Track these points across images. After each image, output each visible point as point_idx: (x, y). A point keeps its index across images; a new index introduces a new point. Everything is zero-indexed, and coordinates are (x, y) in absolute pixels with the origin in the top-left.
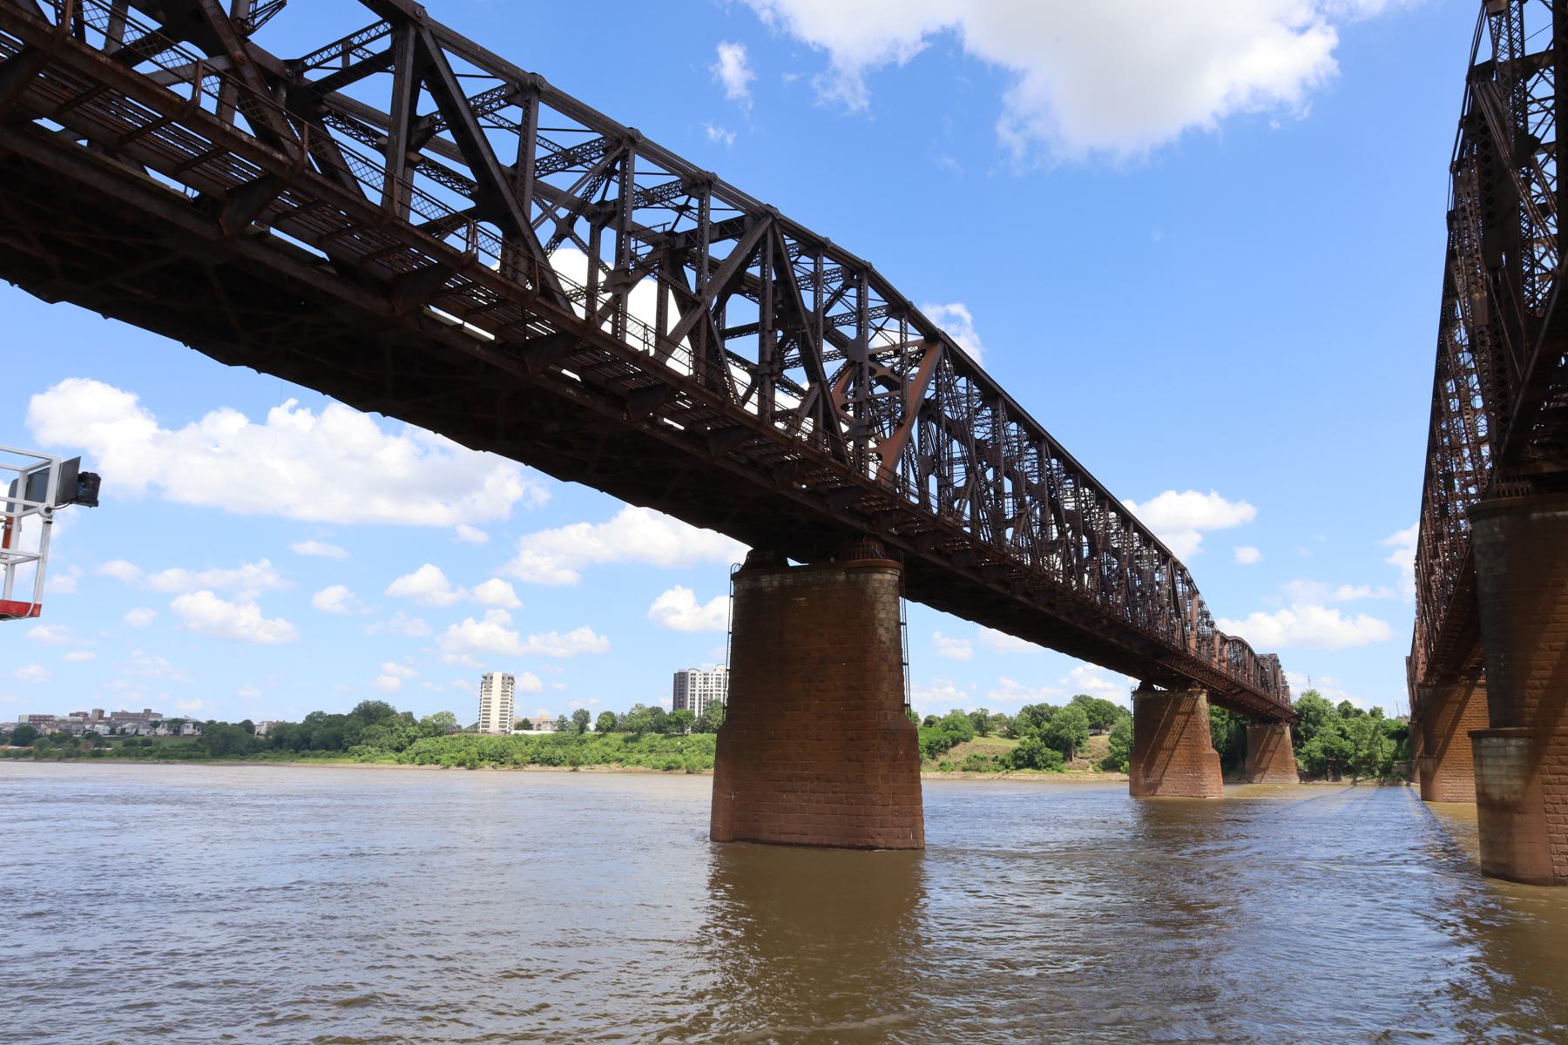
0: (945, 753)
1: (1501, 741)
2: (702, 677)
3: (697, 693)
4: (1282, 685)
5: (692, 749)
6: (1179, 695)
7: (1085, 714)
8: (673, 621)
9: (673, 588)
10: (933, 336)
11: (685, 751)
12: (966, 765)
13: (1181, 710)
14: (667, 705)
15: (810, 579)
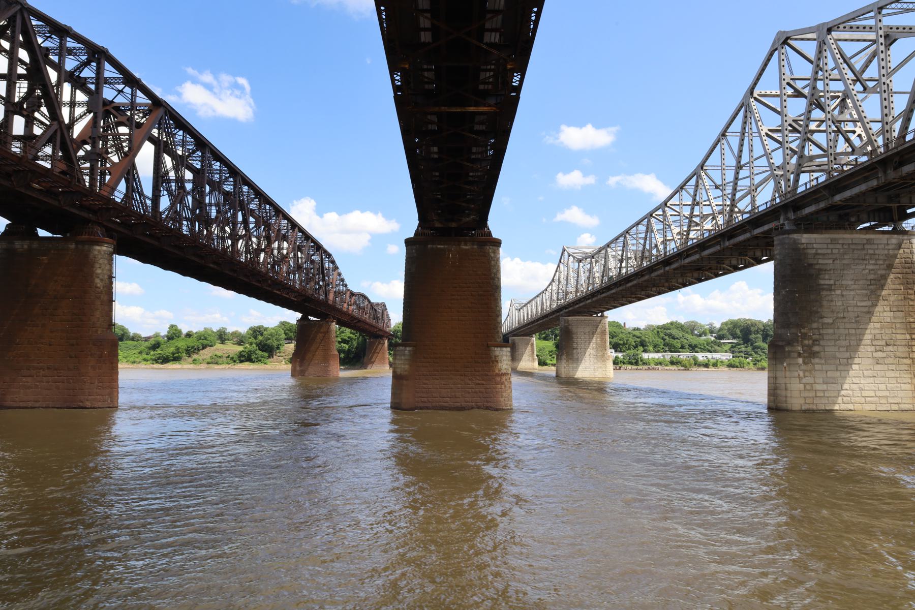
0: (197, 353)
1: (403, 348)
4: (386, 318)
7: (283, 332)
12: (210, 360)
13: (322, 331)
15: (50, 246)
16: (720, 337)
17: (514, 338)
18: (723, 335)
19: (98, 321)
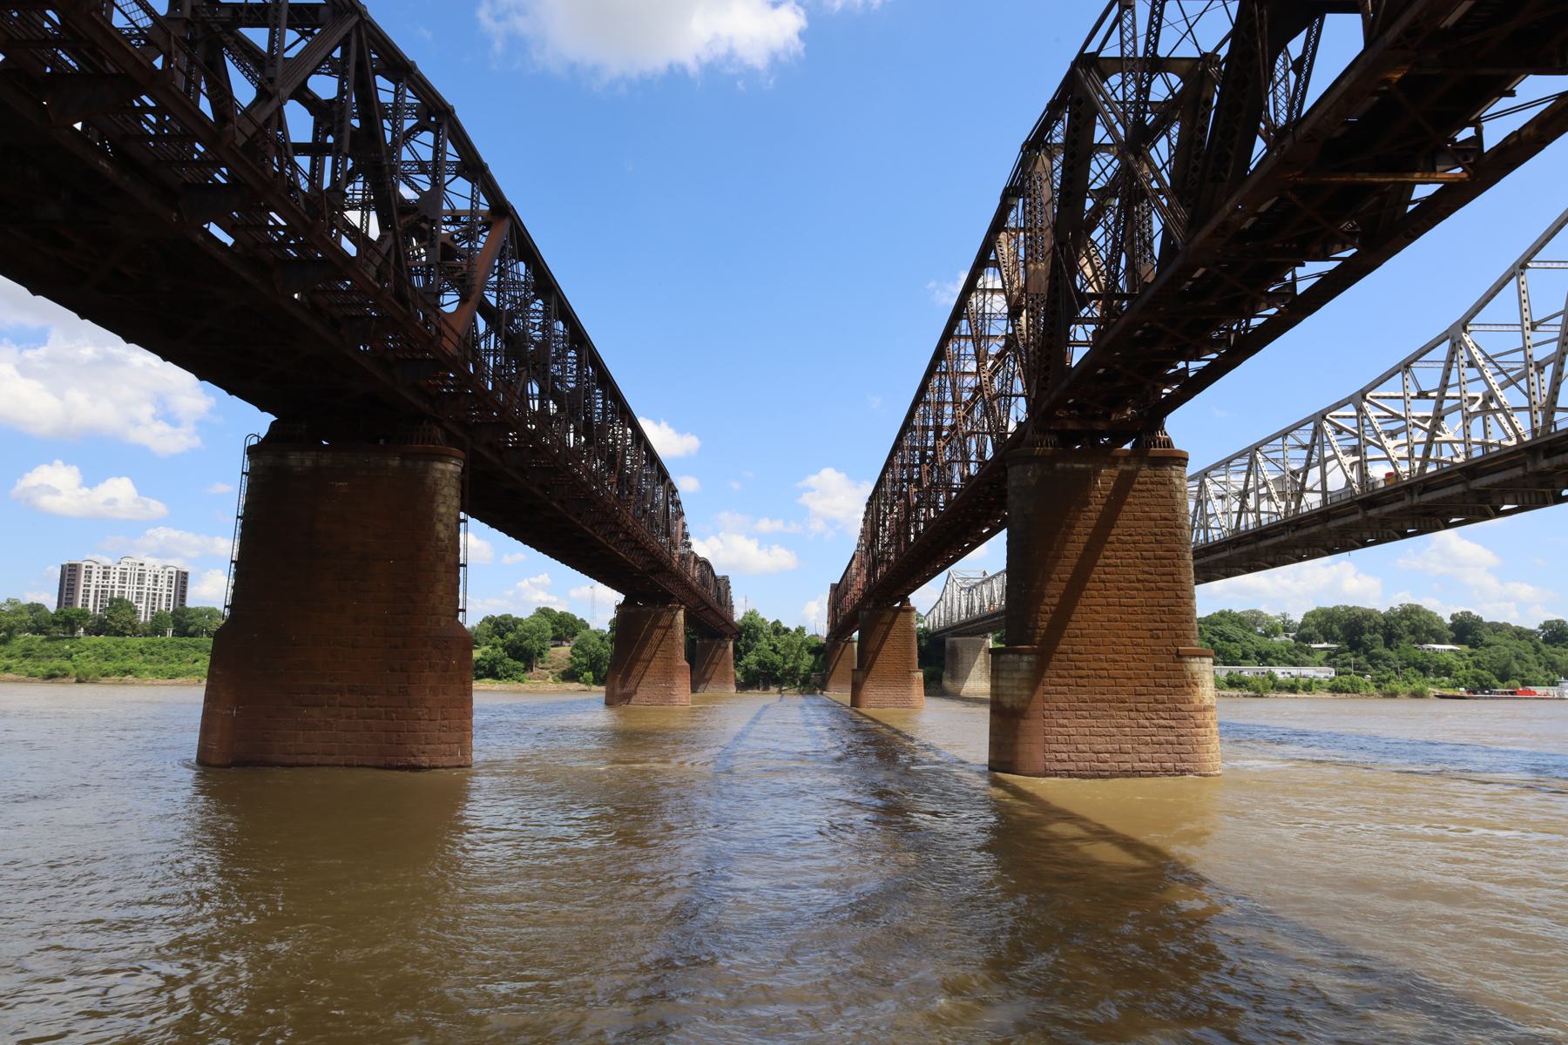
1: (1016, 657)
2: (102, 570)
3: (92, 589)
5: (86, 653)
6: (660, 610)
7: (550, 626)
8: (46, 501)
9: (51, 464)
10: (501, 210)
11: (75, 656)
14: (51, 602)
16: (1308, 638)
17: (954, 639)
18: (1310, 635)
19: (441, 603)
